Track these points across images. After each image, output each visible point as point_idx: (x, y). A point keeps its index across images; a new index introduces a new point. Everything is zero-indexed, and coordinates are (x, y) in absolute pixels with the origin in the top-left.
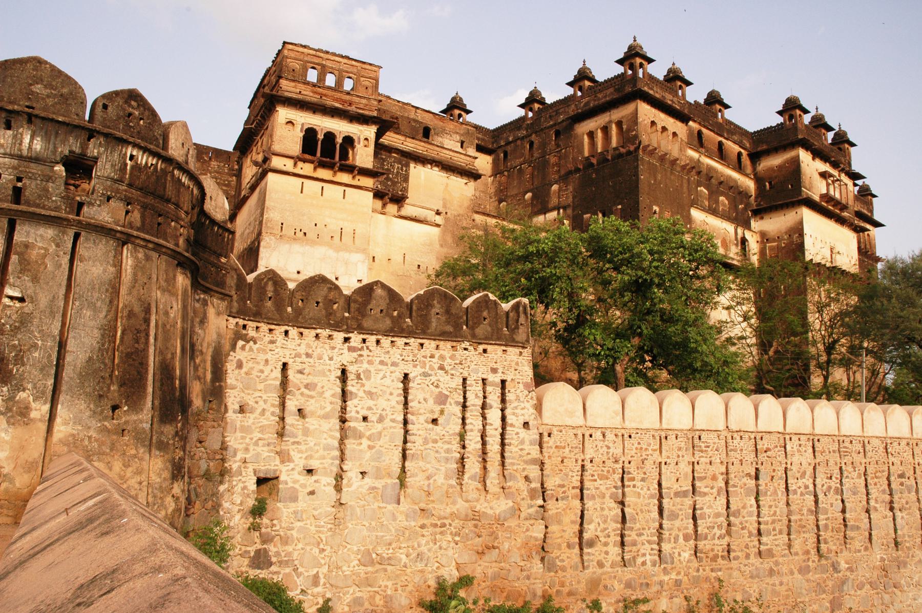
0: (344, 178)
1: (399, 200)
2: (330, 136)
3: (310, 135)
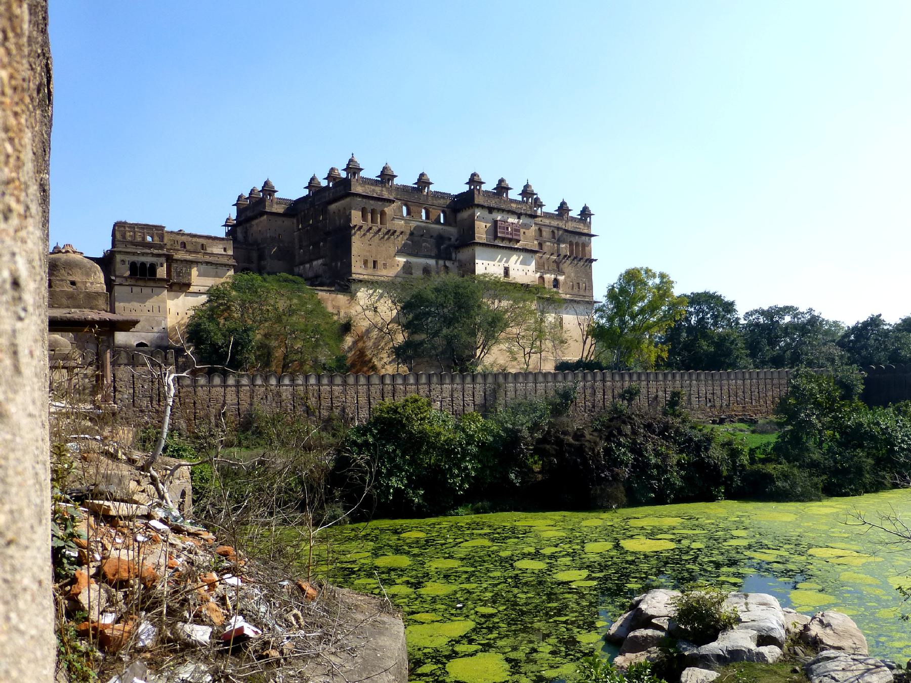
0: (152, 284)
1: (189, 285)
2: (143, 264)
3: (133, 266)
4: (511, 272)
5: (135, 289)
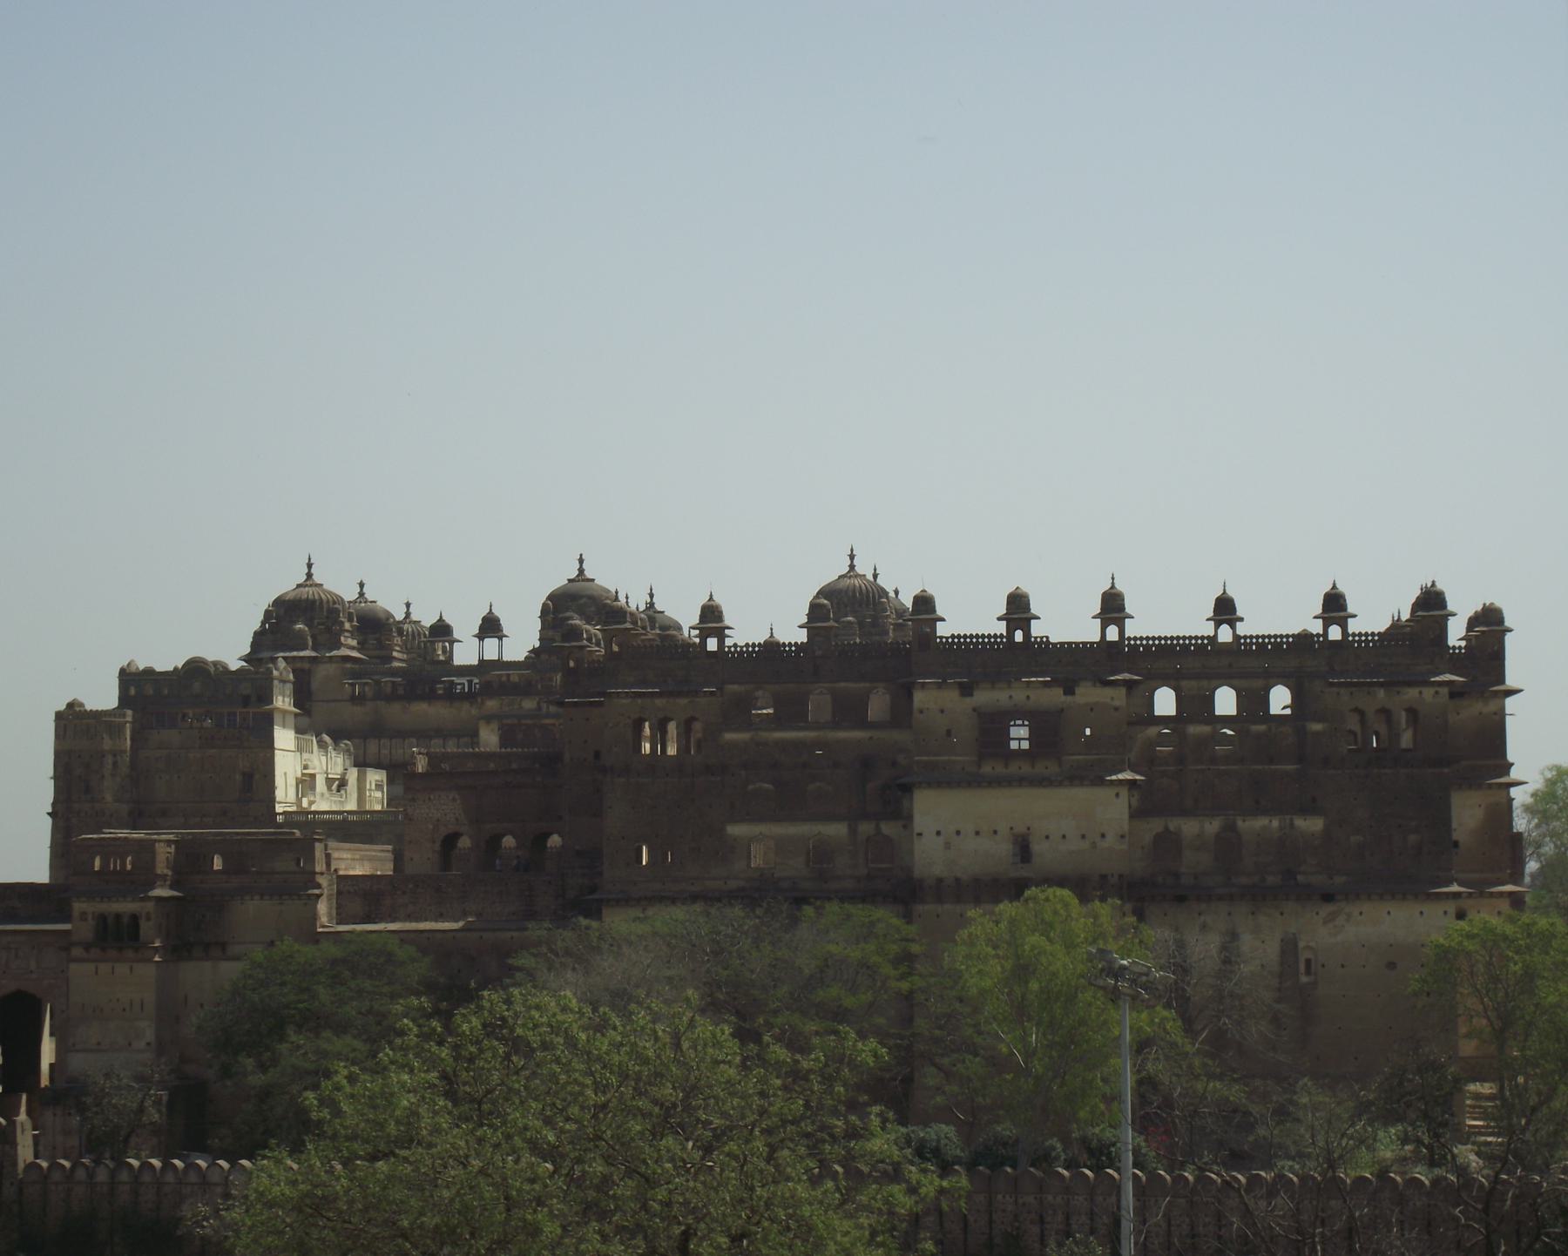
1: (223, 946)
2: (118, 916)
4: (1037, 847)
5: (104, 968)
